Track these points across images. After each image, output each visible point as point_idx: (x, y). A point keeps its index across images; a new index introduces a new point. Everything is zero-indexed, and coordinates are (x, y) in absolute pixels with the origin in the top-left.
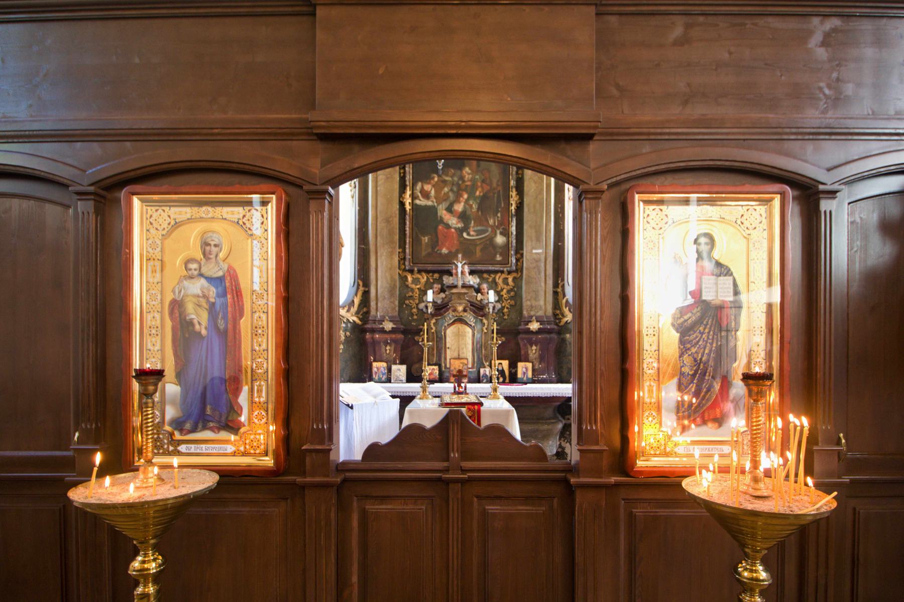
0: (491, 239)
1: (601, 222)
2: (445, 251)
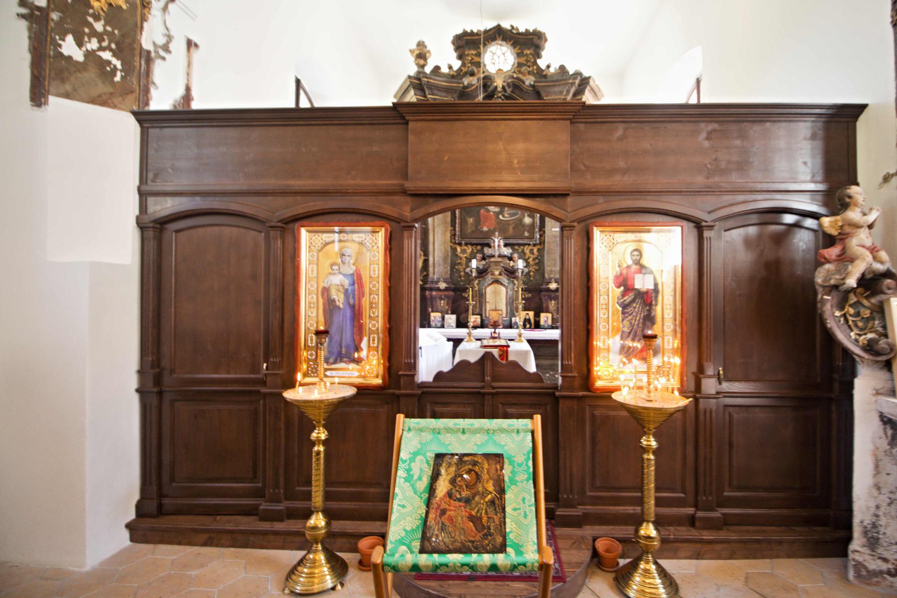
0: (521, 220)
1: (574, 244)
2: (485, 229)
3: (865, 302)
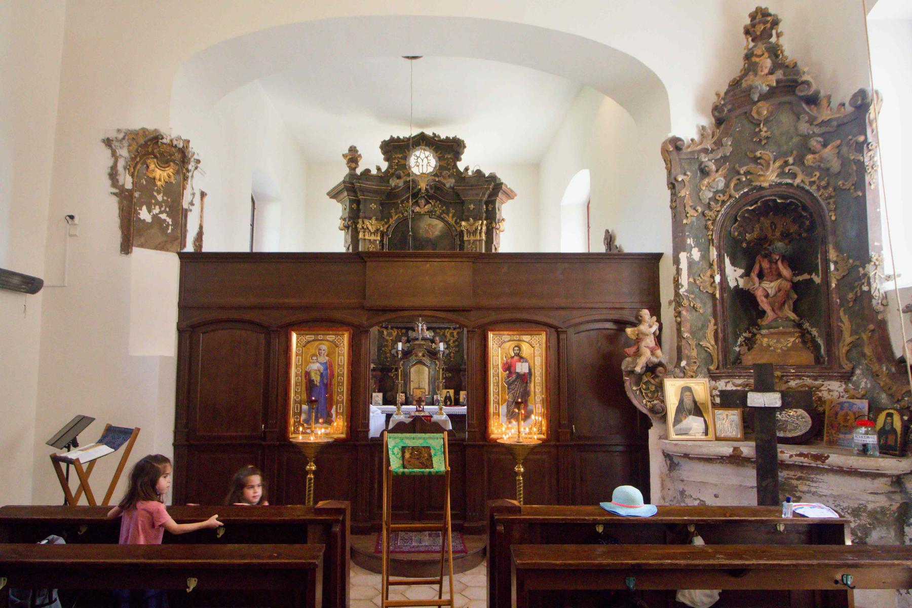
3: (652, 381)
